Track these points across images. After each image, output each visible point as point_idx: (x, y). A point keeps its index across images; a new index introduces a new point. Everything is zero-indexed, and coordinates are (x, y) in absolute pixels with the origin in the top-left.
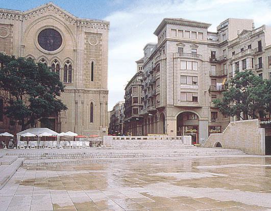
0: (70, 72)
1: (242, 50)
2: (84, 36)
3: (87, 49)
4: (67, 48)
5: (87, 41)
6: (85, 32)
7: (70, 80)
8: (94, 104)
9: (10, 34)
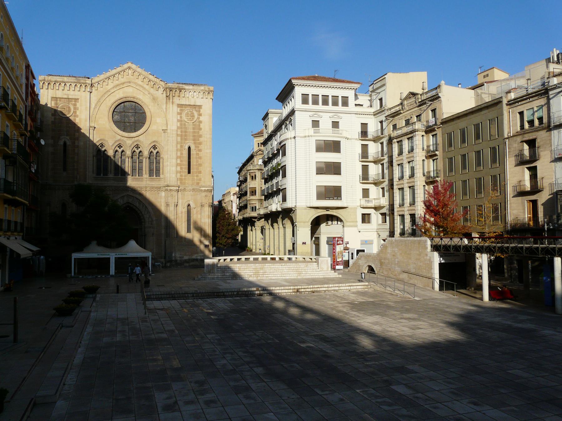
0: (158, 163)
1: (408, 123)
2: (176, 109)
3: (181, 128)
4: (153, 127)
5: (181, 117)
6: (178, 104)
7: (158, 174)
8: (192, 205)
9: (198, 118)
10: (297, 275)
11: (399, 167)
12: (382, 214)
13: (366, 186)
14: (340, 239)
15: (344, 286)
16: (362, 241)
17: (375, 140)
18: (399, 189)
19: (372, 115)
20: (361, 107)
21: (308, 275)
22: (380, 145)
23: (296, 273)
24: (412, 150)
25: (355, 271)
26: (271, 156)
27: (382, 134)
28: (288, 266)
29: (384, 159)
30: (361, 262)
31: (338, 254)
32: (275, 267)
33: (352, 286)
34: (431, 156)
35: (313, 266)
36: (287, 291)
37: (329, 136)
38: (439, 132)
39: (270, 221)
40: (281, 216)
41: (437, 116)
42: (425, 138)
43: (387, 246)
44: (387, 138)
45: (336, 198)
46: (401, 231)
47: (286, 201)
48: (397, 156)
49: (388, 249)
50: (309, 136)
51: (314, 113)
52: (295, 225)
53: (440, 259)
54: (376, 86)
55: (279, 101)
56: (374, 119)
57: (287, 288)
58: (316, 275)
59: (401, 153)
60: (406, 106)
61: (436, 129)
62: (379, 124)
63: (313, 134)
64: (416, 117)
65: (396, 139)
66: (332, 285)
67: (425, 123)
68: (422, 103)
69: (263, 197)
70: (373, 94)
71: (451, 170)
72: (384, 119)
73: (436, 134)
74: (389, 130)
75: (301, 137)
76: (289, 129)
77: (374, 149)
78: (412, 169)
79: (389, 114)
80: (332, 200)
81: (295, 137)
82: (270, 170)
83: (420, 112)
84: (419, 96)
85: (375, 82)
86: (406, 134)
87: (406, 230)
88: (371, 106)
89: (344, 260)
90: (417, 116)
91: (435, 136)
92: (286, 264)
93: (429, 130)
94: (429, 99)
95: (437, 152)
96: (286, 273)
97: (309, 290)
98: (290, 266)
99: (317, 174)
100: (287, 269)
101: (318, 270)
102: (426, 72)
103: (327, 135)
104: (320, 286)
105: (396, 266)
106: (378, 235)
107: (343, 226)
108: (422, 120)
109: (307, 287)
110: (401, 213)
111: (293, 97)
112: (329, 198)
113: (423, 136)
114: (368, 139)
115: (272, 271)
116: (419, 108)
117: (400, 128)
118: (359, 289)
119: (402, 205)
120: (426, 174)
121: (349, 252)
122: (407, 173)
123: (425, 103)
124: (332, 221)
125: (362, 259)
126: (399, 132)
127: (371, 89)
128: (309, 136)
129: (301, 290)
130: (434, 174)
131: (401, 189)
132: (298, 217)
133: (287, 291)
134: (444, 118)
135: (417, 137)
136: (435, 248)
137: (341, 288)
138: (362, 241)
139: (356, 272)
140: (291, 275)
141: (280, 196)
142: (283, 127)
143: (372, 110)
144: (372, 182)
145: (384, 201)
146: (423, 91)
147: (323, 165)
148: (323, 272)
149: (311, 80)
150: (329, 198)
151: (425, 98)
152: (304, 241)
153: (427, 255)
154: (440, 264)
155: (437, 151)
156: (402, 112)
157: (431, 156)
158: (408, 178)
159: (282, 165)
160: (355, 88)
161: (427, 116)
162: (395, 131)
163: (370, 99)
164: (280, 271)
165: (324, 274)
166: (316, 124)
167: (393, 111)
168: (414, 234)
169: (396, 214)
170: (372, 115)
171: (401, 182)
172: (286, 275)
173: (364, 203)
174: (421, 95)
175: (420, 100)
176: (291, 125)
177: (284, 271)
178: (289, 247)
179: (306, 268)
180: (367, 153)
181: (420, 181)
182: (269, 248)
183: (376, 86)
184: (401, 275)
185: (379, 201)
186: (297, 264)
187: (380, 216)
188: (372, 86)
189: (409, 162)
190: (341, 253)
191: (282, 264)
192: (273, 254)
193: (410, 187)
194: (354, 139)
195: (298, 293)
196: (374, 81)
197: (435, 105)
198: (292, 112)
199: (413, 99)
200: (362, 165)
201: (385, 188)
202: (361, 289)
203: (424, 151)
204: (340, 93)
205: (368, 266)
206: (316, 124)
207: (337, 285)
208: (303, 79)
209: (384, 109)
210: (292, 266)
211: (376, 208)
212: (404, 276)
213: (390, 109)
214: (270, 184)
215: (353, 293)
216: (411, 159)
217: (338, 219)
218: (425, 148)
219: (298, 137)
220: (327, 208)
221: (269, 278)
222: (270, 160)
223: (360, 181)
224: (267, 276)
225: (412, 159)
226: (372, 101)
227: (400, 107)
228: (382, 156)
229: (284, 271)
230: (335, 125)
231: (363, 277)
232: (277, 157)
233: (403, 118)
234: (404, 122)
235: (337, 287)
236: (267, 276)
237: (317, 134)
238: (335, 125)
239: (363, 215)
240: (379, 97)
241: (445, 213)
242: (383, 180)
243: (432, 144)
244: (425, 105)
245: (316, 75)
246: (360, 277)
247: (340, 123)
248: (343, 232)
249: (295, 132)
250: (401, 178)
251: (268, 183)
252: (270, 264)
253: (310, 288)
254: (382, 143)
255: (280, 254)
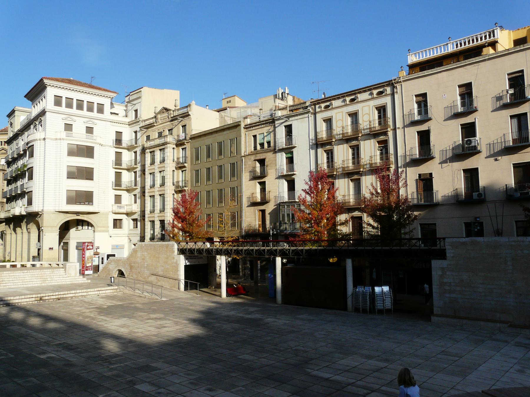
1: (160, 135)
10: (41, 282)
11: (151, 176)
12: (133, 220)
13: (119, 193)
14: (90, 244)
15: (92, 291)
16: (112, 246)
17: (129, 149)
18: (150, 196)
19: (127, 124)
20: (117, 116)
21: (54, 281)
22: (134, 154)
23: (40, 280)
24: (163, 161)
25: (105, 276)
26: (16, 156)
27: (136, 144)
28: (31, 273)
29: (137, 168)
30: (111, 267)
31: (88, 259)
32: (15, 274)
33: (101, 290)
34: (180, 168)
35: (60, 272)
36: (28, 300)
37: (82, 141)
38: (188, 146)
39: (12, 226)
40: (25, 220)
41: (187, 132)
42: (175, 150)
43: (137, 250)
44: (141, 148)
45: (87, 203)
46: (151, 236)
47: (32, 205)
48: (149, 165)
49: (138, 253)
50: (60, 139)
51: (68, 116)
52: (41, 230)
53: (186, 262)
54: (132, 98)
55: (28, 99)
56: (128, 128)
57: (29, 296)
58: (62, 281)
59: (153, 163)
60: (159, 120)
61: (185, 143)
62: (134, 134)
63: (64, 137)
64: (168, 131)
65: (149, 149)
66: (80, 291)
67: (176, 137)
68: (174, 119)
69: (5, 200)
70: (129, 105)
71: (197, 181)
72: (138, 129)
73: (185, 148)
74: (142, 140)
75: (52, 139)
76: (39, 130)
77: (127, 157)
78: (163, 178)
79: (144, 125)
80: (83, 205)
81: (44, 139)
82: (15, 171)
83: (172, 126)
84: (172, 112)
85: (131, 94)
86: (158, 146)
87: (155, 235)
88: (126, 116)
89: (94, 265)
90: (169, 130)
91: (184, 149)
92: (28, 271)
93: (179, 144)
94: (180, 116)
95: (185, 164)
96: (28, 280)
97: (54, 297)
98: (33, 273)
99: (68, 178)
100: (30, 276)
101: (65, 276)
102: (179, 91)
103: (80, 139)
104: (66, 293)
105: (145, 269)
106: (129, 240)
107: (94, 231)
108: (174, 134)
109: (52, 294)
110: (152, 219)
111: (45, 97)
112: (80, 203)
113: (173, 148)
114: (122, 147)
115: (11, 279)
116: (171, 123)
117: (153, 140)
118: (108, 293)
119: (152, 212)
120: (175, 183)
121: (99, 257)
122: (158, 182)
123: (177, 119)
124: (82, 226)
125: (111, 264)
126: (152, 143)
127: (127, 99)
128: (60, 139)
129: (44, 298)
130: (182, 184)
131: (153, 197)
132: (44, 221)
133: (28, 300)
134: (193, 134)
135: (168, 149)
136: (182, 251)
137: (89, 293)
138: (112, 246)
139: (105, 277)
140: (33, 283)
141: (25, 200)
142: (32, 126)
143: (127, 120)
144: (124, 188)
145: (136, 208)
146: (175, 107)
147: (74, 170)
148: (71, 278)
149: (66, 82)
150: (80, 203)
151: (177, 115)
152: (51, 247)
153: (174, 258)
154: (186, 266)
155: (186, 163)
156: (155, 124)
157: (181, 167)
158: (159, 186)
159: (29, 166)
160: (112, 97)
161: (178, 130)
162: (148, 142)
163: (125, 109)
164: (21, 279)
165: (71, 280)
166: (68, 127)
167: (147, 122)
168: (163, 238)
169: (146, 220)
170: (127, 124)
171: (152, 190)
172: (29, 283)
173: (116, 208)
174: (173, 111)
175: (172, 116)
176: (41, 126)
177: (26, 278)
178: (34, 252)
179: (52, 275)
180: (121, 160)
181: (170, 190)
182: (9, 255)
183: (132, 98)
184: (150, 278)
185: (131, 207)
186: (42, 271)
187: (132, 222)
188: (129, 97)
189: (160, 172)
190: (91, 258)
191: (23, 271)
192: (15, 260)
193: (160, 195)
194: (108, 146)
195: (41, 301)
196: (130, 93)
197: (185, 121)
198: (43, 113)
199: (166, 114)
200: (115, 172)
201: (137, 195)
202: (110, 293)
203: (175, 163)
204: (96, 100)
205: (118, 270)
206: (68, 127)
207: (85, 291)
208: (57, 80)
209: (138, 120)
210: (35, 273)
211: (128, 214)
212: (153, 279)
213: (145, 121)
214: (13, 186)
215: (102, 298)
216: (162, 169)
217: (89, 224)
218: (176, 160)
219: (49, 138)
220: (78, 213)
221: (7, 287)
222: (15, 160)
223: (112, 187)
224: (5, 285)
225: (163, 169)
226: (128, 111)
227: (154, 120)
228: (136, 164)
229: (26, 278)
230: (90, 130)
231: (113, 281)
232: (23, 158)
233: (157, 130)
234: (157, 134)
235: (86, 292)
236: (5, 285)
237: (69, 138)
238: (90, 130)
239: (115, 220)
240: (135, 109)
241: (191, 219)
242: (135, 187)
243: (181, 156)
244: (177, 121)
245: (72, 79)
246: (109, 281)
247: (73, 126)
248: (94, 237)
249: (45, 133)
250: (153, 186)
251: (11, 184)
252: (9, 272)
253: (55, 295)
254: (135, 152)
255: (23, 260)
